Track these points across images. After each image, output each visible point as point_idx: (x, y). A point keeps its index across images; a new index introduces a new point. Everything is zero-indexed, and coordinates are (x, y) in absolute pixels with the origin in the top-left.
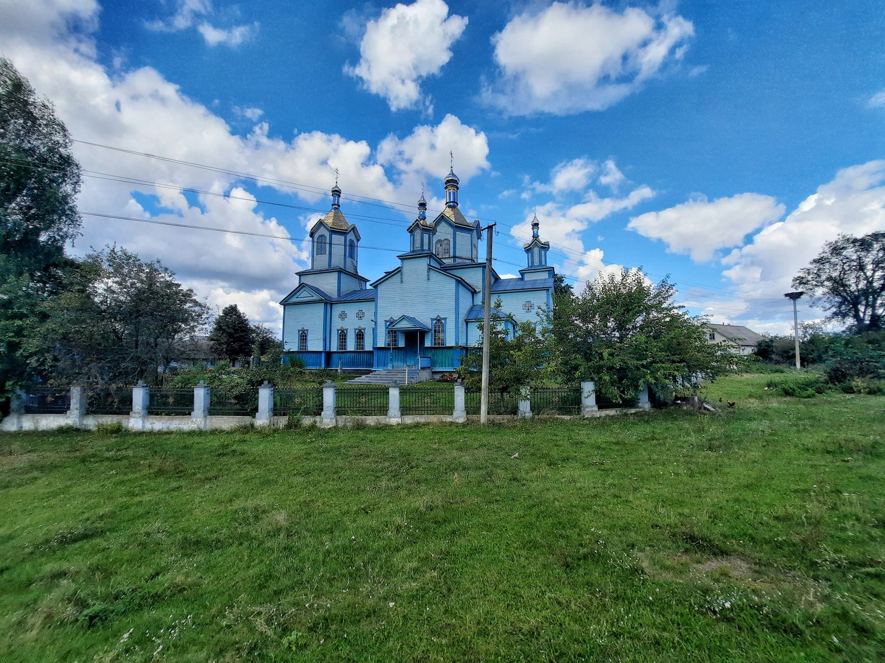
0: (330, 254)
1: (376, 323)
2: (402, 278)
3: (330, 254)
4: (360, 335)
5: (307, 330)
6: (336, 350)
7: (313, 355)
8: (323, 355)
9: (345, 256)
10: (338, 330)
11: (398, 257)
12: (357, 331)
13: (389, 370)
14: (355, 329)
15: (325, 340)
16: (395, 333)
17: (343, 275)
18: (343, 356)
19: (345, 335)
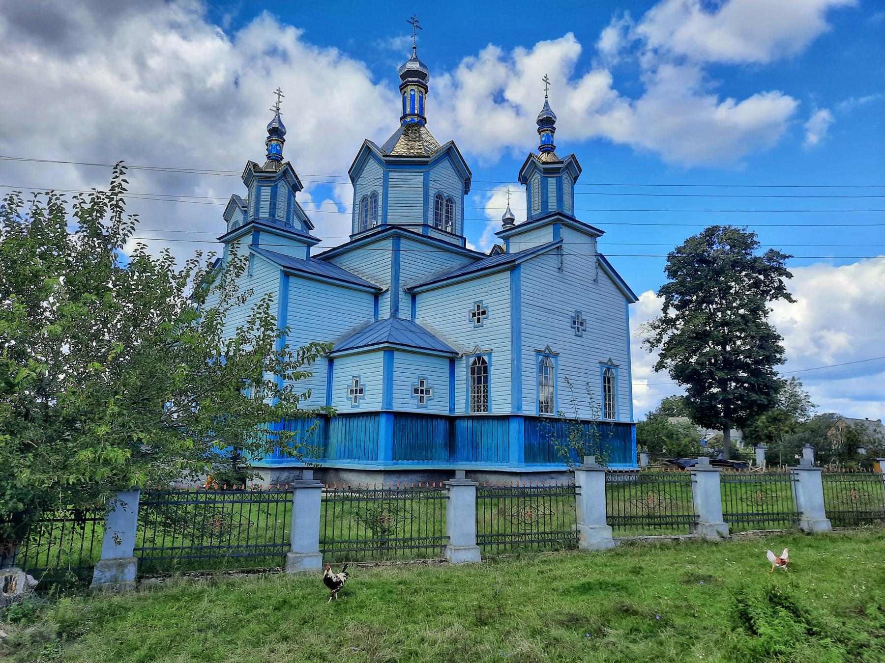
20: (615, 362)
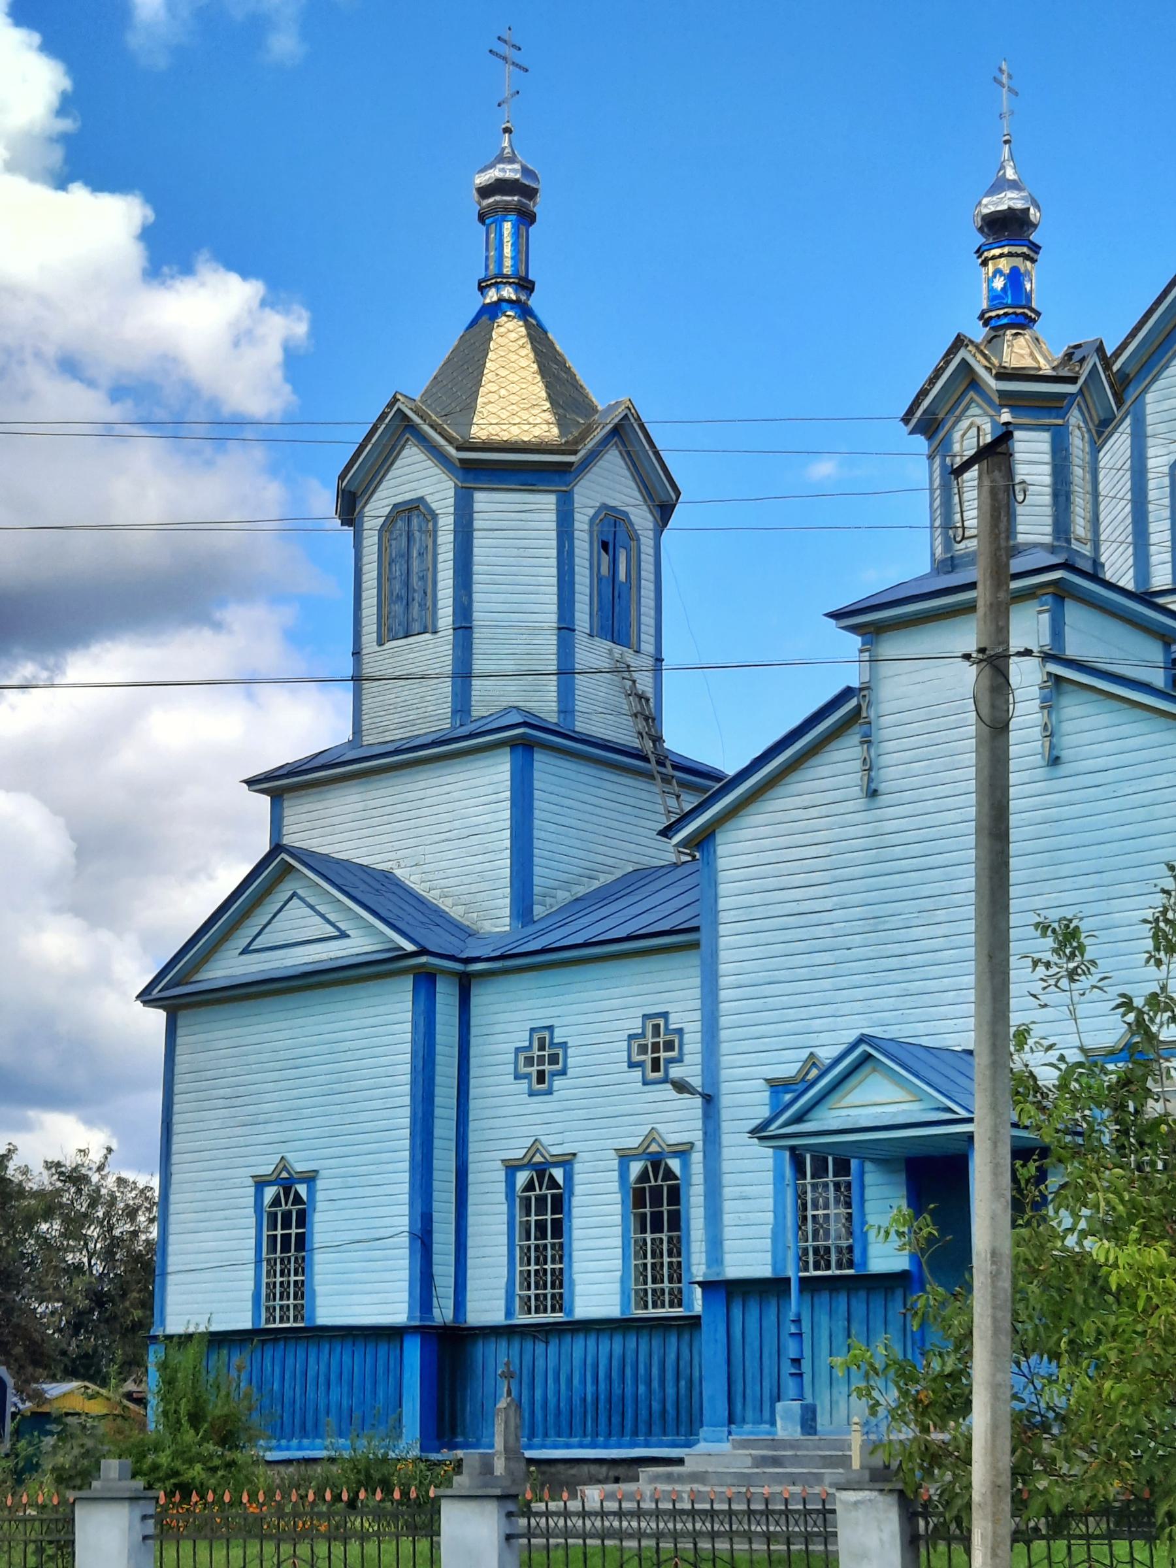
0: (464, 627)
1: (710, 1100)
2: (869, 767)
3: (464, 627)
4: (656, 1192)
5: (310, 1178)
6: (496, 1317)
7: (345, 1357)
8: (413, 1350)
9: (566, 628)
10: (511, 1168)
11: (836, 615)
12: (636, 1168)
13: (775, 1444)
14: (625, 1157)
15: (422, 1238)
16: (843, 1167)
17: (545, 767)
18: (546, 1355)
19: (559, 1204)
20: (300, 1167)
